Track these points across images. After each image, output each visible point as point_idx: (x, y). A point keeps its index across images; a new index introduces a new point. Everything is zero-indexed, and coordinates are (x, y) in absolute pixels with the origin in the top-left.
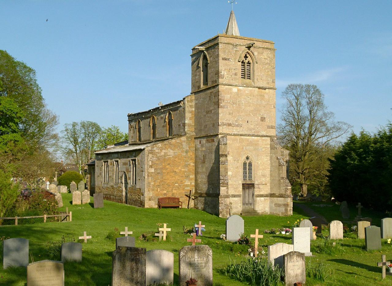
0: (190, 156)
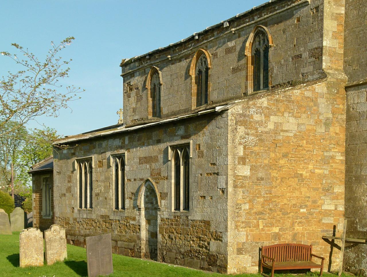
0: (334, 135)
